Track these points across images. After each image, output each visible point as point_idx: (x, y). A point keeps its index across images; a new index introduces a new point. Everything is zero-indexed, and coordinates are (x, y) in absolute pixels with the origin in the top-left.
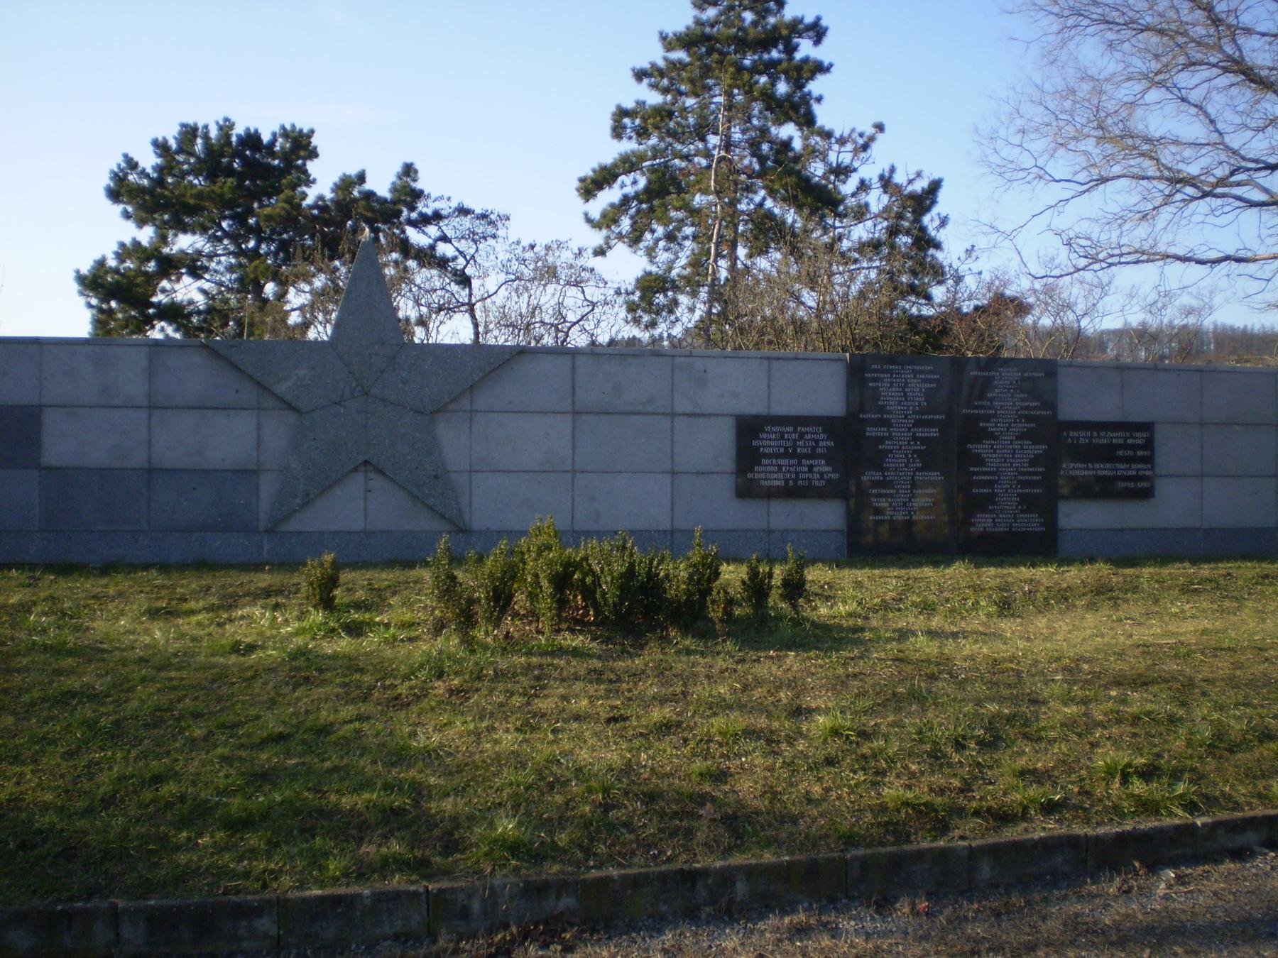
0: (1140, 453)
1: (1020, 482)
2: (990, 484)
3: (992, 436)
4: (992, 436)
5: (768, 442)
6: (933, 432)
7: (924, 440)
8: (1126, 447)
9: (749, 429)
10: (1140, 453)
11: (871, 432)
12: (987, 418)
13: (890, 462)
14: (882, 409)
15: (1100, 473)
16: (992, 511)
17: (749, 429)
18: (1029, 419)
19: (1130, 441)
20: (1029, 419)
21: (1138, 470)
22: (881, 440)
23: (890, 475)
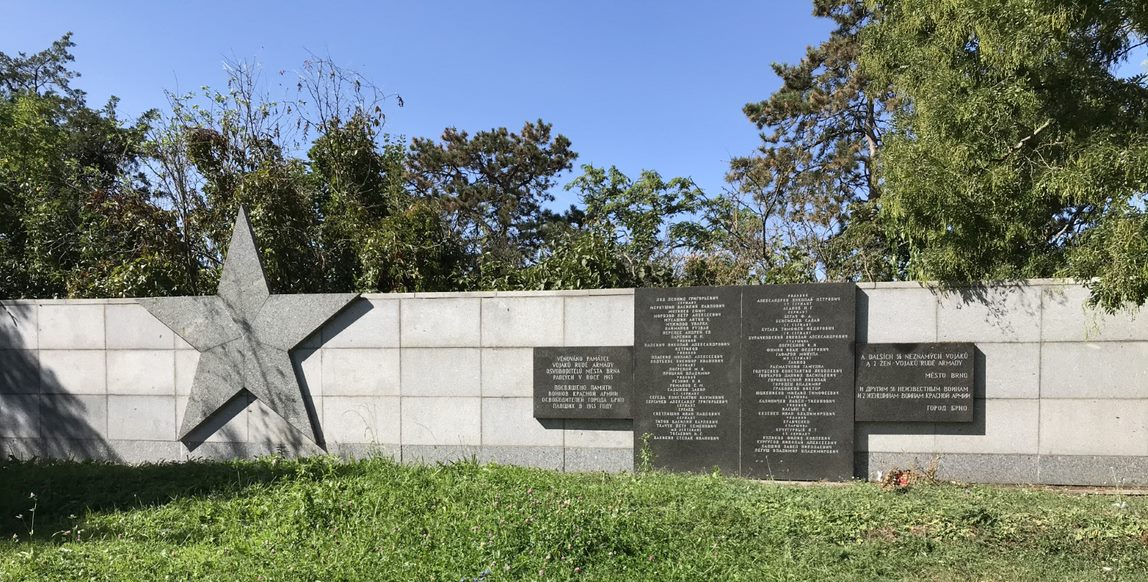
2: (777, 407)
3: (780, 361)
4: (780, 361)
5: (560, 370)
6: (717, 359)
7: (707, 367)
8: (936, 369)
9: (545, 358)
11: (657, 359)
12: (775, 344)
13: (673, 386)
14: (667, 339)
17: (545, 358)
18: (821, 343)
20: (821, 343)
21: (951, 393)
22: (665, 367)
23: (674, 400)
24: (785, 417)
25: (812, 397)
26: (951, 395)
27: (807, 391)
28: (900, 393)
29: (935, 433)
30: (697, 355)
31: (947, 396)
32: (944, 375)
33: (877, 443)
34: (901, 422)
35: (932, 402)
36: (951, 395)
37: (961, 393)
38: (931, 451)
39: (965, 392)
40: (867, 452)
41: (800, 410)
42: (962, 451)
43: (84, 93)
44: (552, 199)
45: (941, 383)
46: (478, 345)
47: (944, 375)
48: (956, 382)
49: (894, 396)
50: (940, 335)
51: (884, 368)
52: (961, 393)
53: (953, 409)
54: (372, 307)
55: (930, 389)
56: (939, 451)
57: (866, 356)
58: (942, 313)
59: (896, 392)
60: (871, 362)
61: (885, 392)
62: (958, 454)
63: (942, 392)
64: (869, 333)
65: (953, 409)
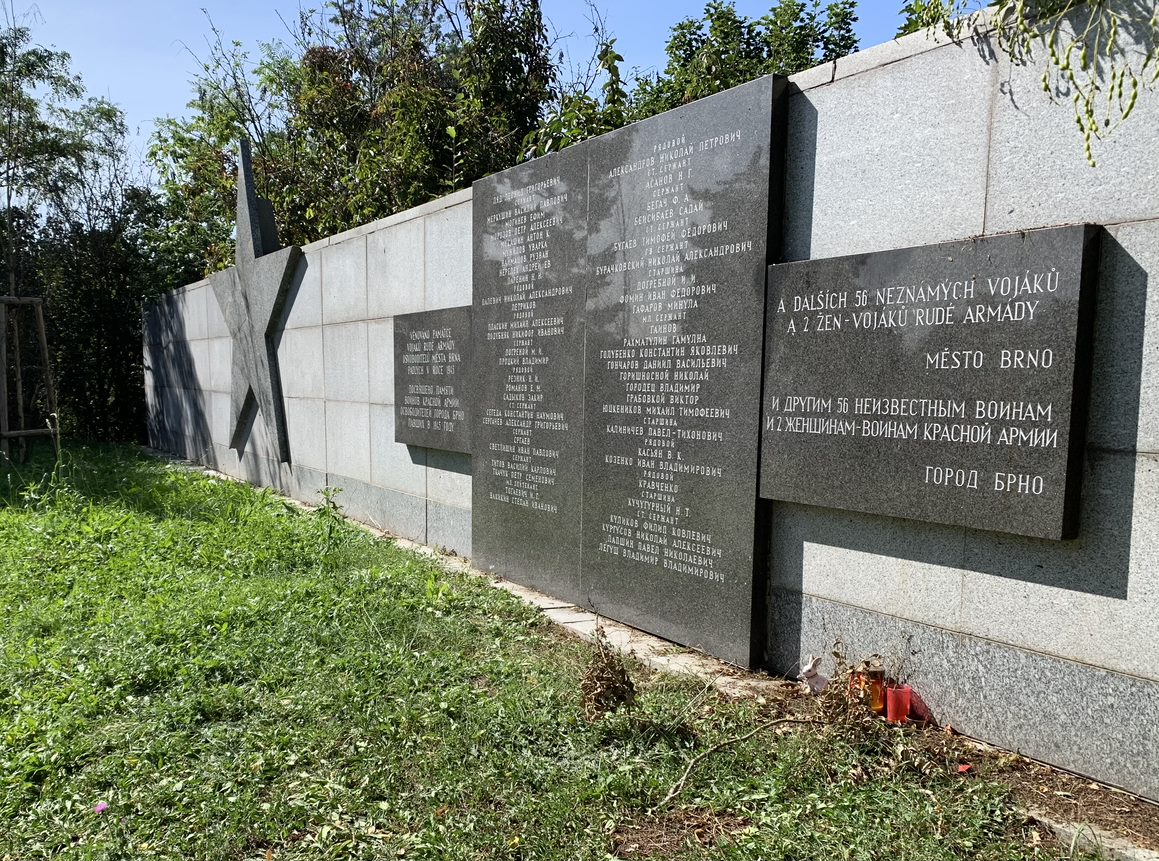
0: (1011, 359)
1: (681, 444)
10: (1011, 359)
15: (869, 429)
16: (632, 512)
19: (975, 316)
21: (998, 425)
24: (641, 470)
25: (686, 423)
26: (996, 433)
27: (677, 406)
28: (859, 419)
29: (965, 562)
30: (535, 317)
31: (984, 435)
32: (978, 359)
33: (828, 571)
34: (884, 517)
35: (937, 452)
36: (996, 433)
37: (1027, 425)
38: (949, 623)
39: (1041, 424)
40: (800, 593)
41: (665, 459)
42: (1042, 644)
43: (65, 56)
44: (255, 72)
45: (963, 387)
46: (328, 330)
47: (978, 359)
48: (1013, 386)
49: (844, 428)
50: (998, 206)
51: (827, 337)
52: (1027, 425)
53: (998, 485)
54: (1125, 597)
55: (939, 409)
56: (972, 626)
57: (789, 305)
58: (1009, 124)
59: (850, 417)
60: (798, 318)
61: (824, 414)
62: (1031, 653)
63: (970, 420)
64: (815, 230)
65: (998, 485)
